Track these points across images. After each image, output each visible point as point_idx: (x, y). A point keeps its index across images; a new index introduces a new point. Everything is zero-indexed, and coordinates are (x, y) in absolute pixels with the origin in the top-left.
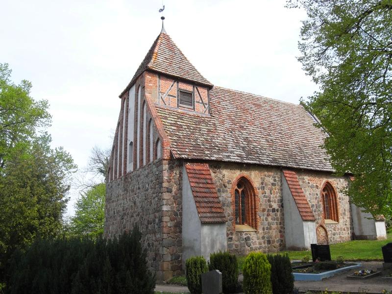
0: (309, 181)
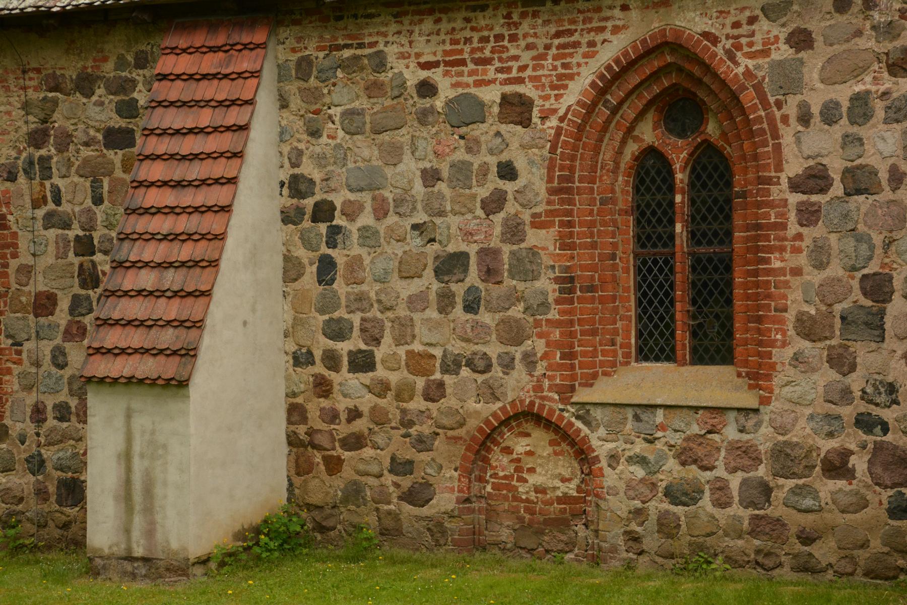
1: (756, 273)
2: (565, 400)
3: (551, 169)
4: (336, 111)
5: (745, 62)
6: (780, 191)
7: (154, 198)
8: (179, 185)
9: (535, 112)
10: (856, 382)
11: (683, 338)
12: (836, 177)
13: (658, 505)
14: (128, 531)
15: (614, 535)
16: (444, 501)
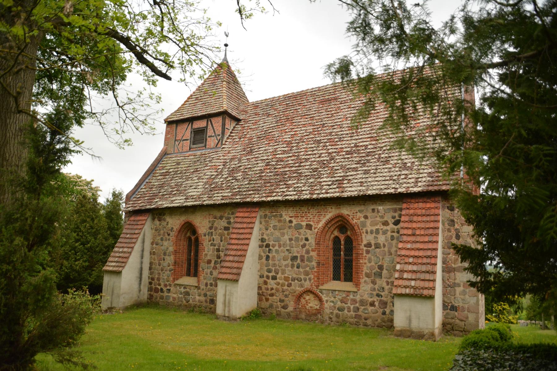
0: (293, 219)
1: (357, 263)
2: (317, 288)
3: (316, 239)
4: (272, 225)
5: (355, 221)
6: (362, 247)
7: (233, 241)
8: (239, 239)
9: (313, 228)
10: (376, 287)
11: (342, 276)
12: (373, 245)
13: (336, 311)
14: (224, 311)
15: (326, 317)
16: (290, 309)
